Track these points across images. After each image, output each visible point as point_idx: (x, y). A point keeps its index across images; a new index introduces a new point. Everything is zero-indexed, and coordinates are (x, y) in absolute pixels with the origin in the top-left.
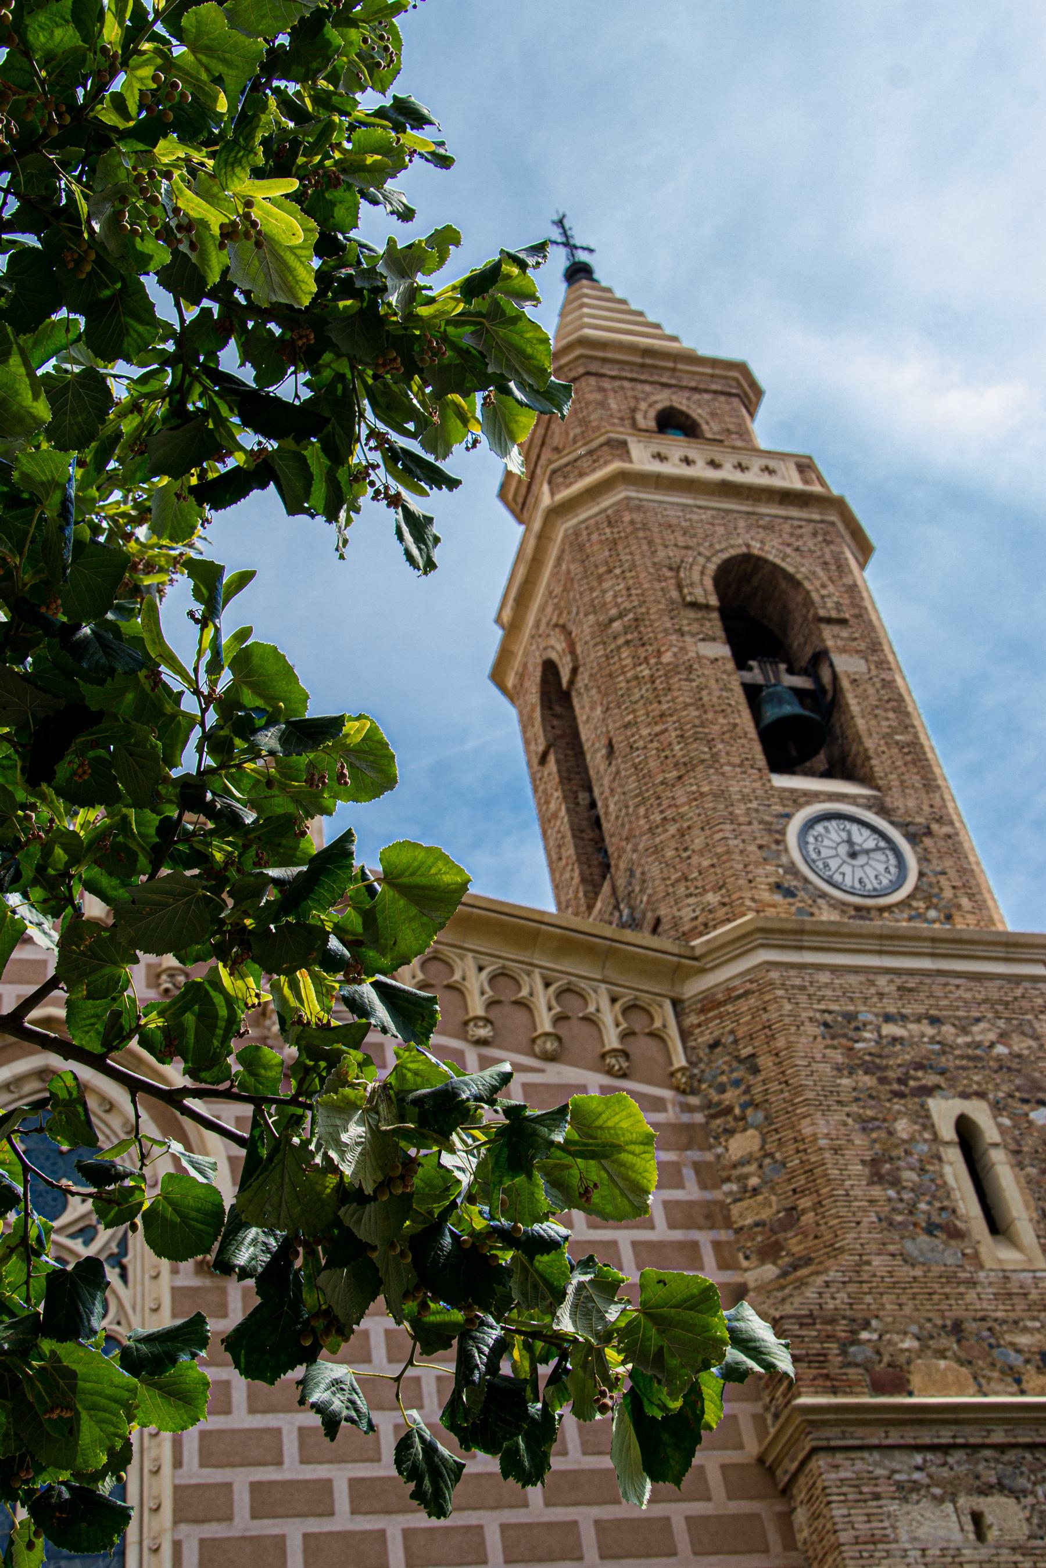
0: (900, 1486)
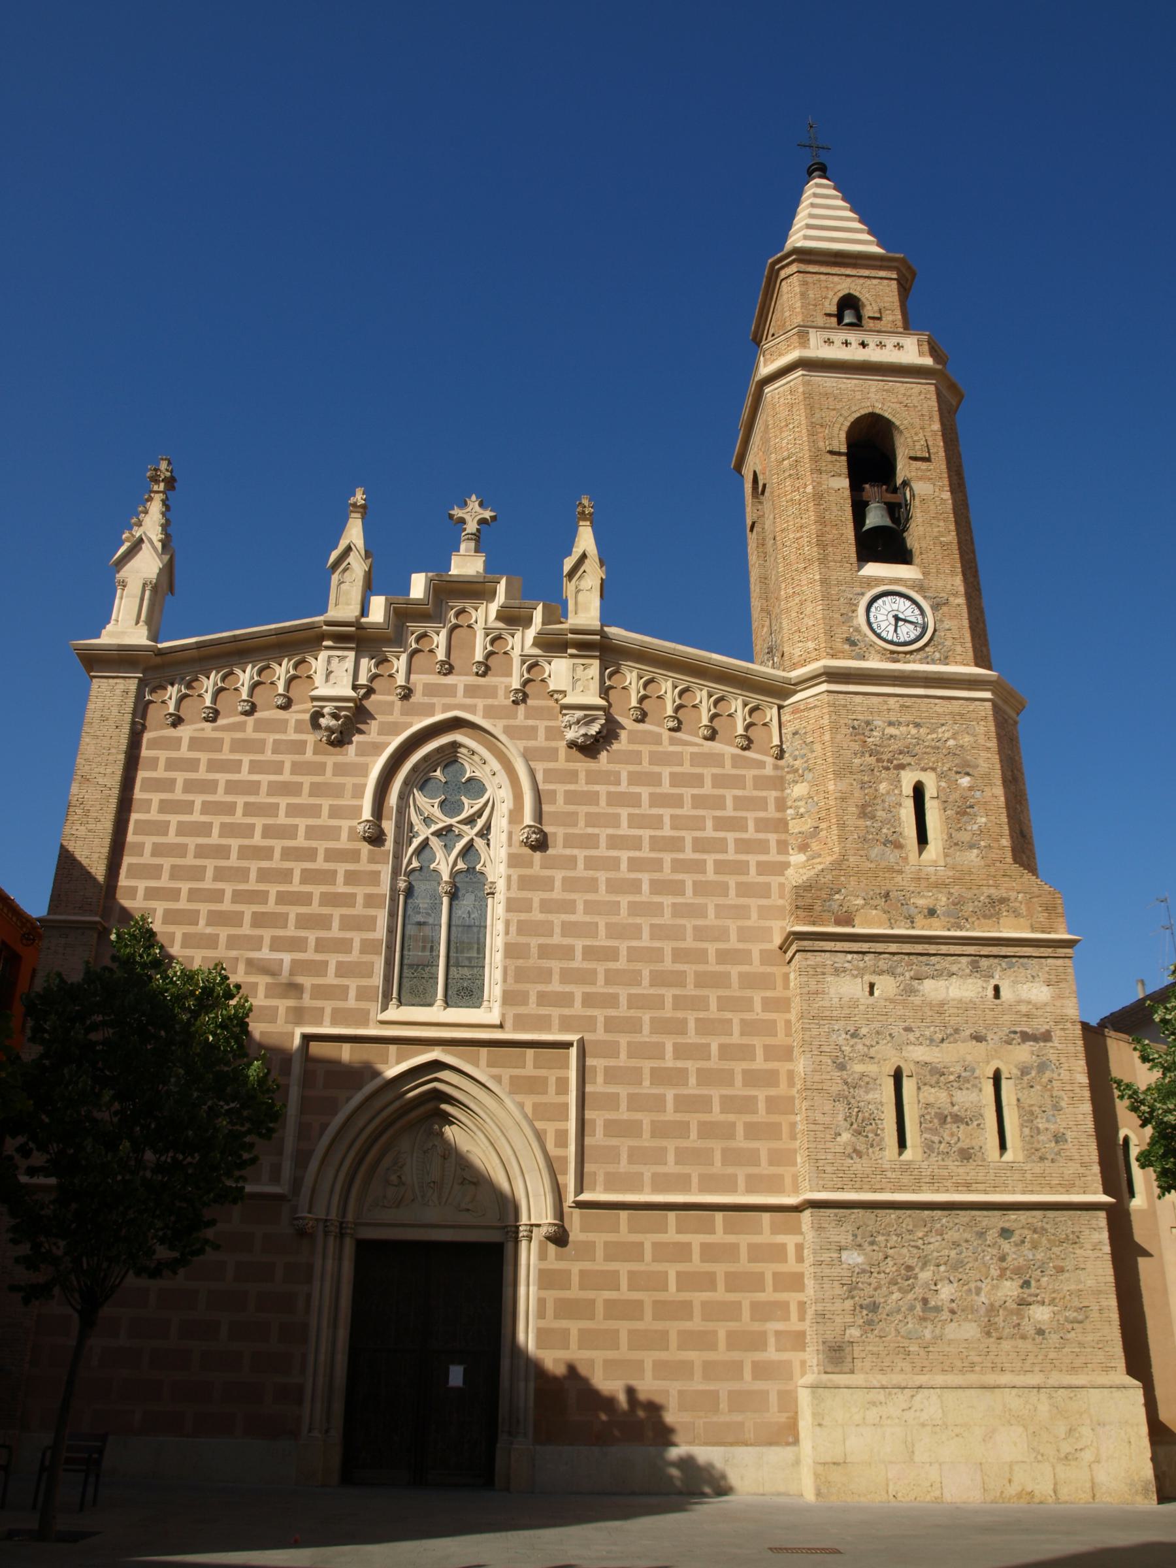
0: (836, 970)
